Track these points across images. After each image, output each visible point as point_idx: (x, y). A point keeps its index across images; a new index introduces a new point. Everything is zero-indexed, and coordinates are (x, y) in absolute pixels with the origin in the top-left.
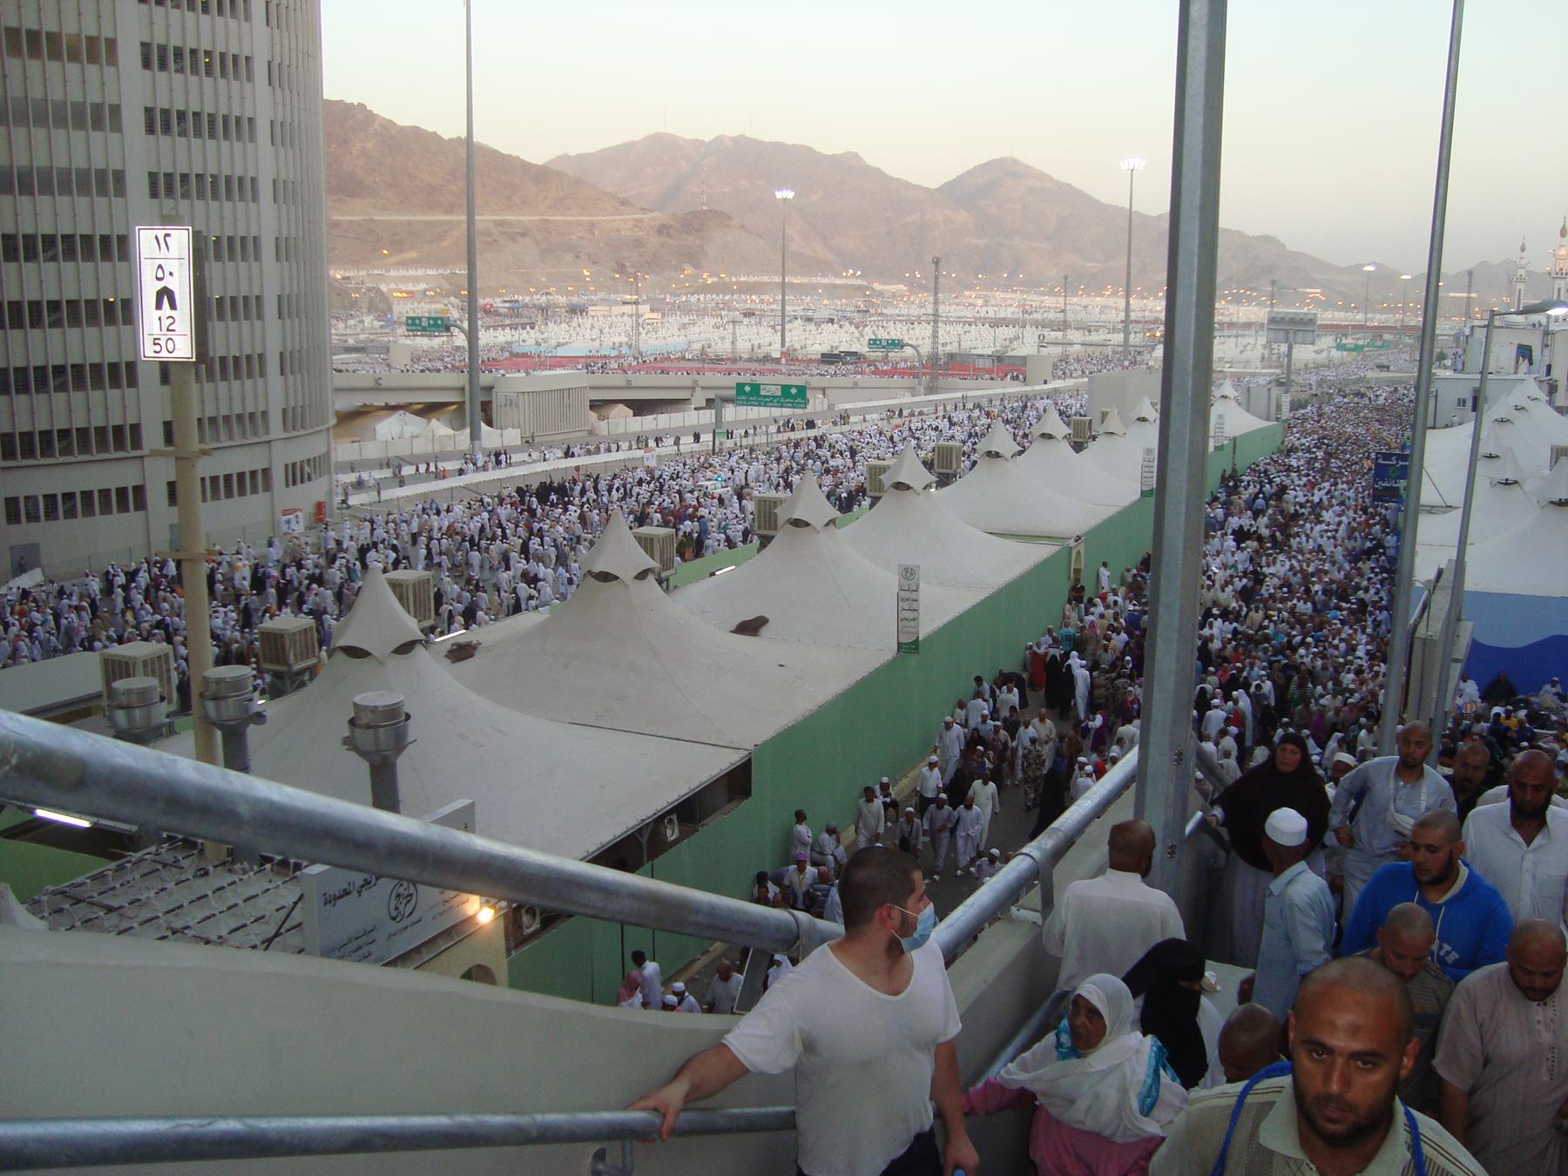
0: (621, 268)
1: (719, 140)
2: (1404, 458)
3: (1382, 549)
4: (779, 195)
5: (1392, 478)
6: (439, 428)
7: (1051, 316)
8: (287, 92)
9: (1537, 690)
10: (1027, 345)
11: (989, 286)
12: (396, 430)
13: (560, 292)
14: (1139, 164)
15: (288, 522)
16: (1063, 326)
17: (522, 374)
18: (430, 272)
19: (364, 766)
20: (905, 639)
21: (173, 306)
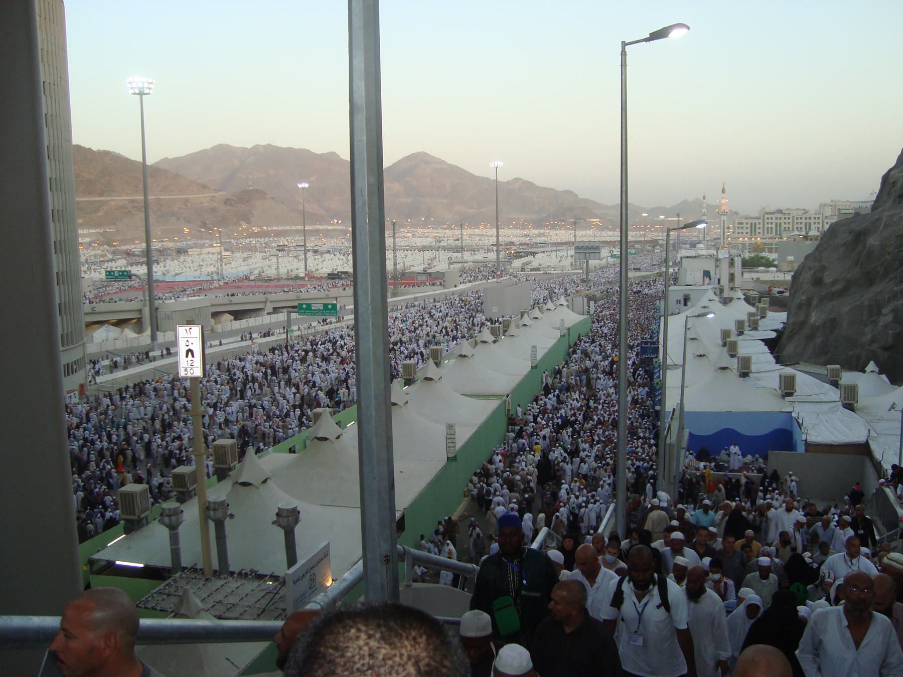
0: (204, 225)
1: (256, 147)
2: (654, 343)
3: (651, 411)
4: (300, 186)
5: (649, 365)
6: (129, 333)
7: (453, 243)
8: (53, 161)
9: (719, 453)
10: (441, 266)
11: (416, 226)
12: (104, 335)
13: (171, 240)
14: (500, 164)
15: (70, 397)
16: (460, 249)
17: (173, 301)
18: (91, 231)
19: (283, 531)
20: (450, 456)
21: (193, 356)
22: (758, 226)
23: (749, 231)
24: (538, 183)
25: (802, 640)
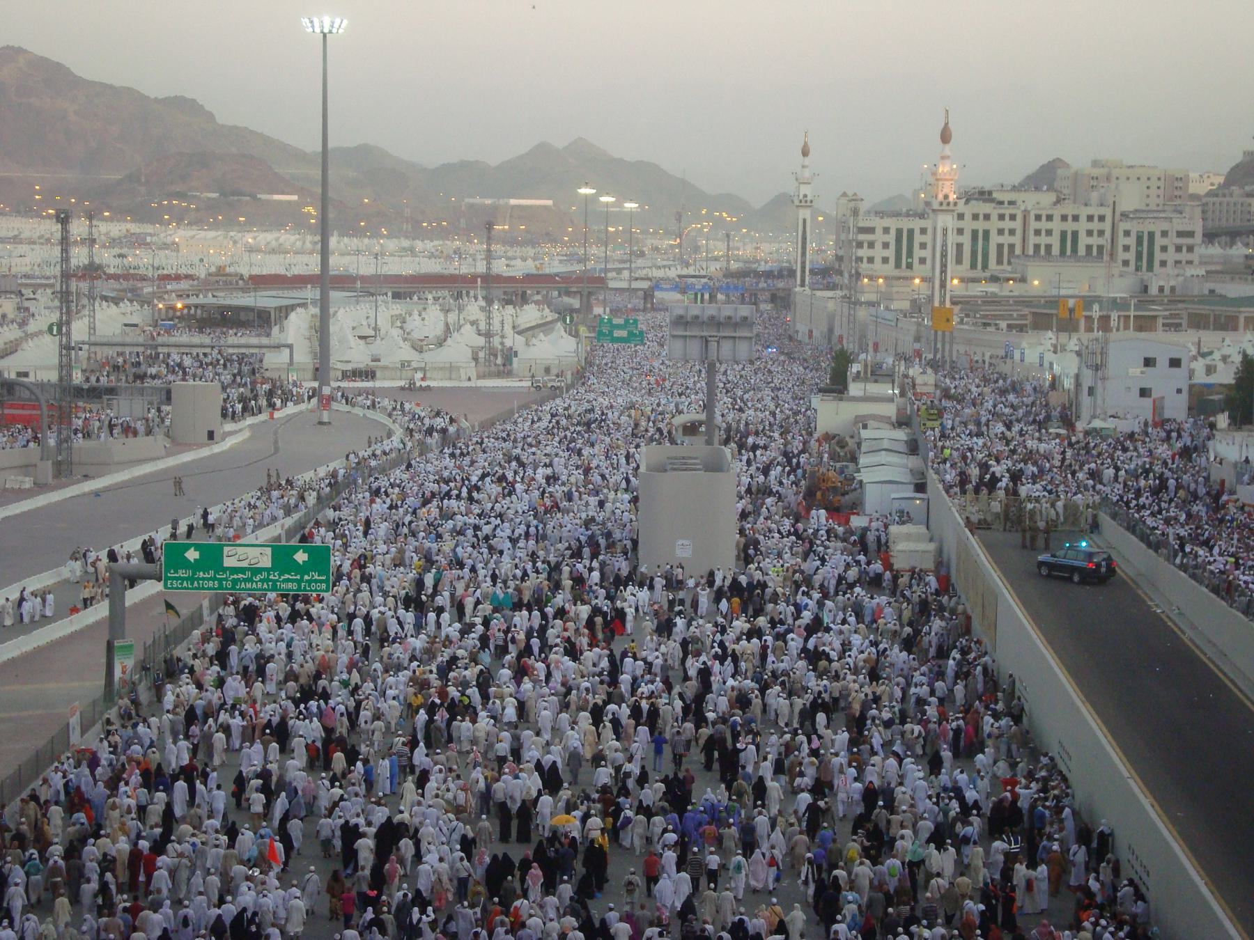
22: (918, 238)
23: (890, 253)
24: (80, 70)
25: (40, 644)
